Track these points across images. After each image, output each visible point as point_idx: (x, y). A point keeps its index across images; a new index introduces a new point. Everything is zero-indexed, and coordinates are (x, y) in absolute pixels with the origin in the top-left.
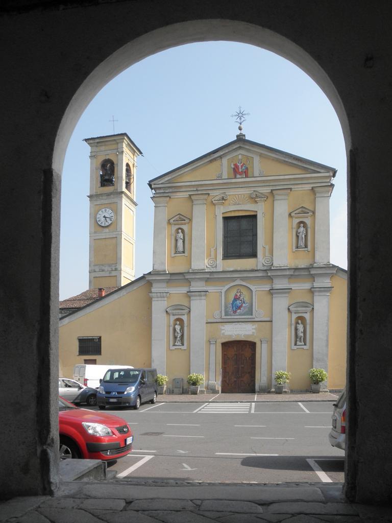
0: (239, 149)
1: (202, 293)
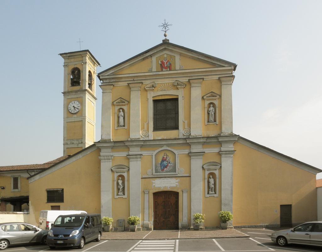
0: (165, 50)
1: (138, 156)
